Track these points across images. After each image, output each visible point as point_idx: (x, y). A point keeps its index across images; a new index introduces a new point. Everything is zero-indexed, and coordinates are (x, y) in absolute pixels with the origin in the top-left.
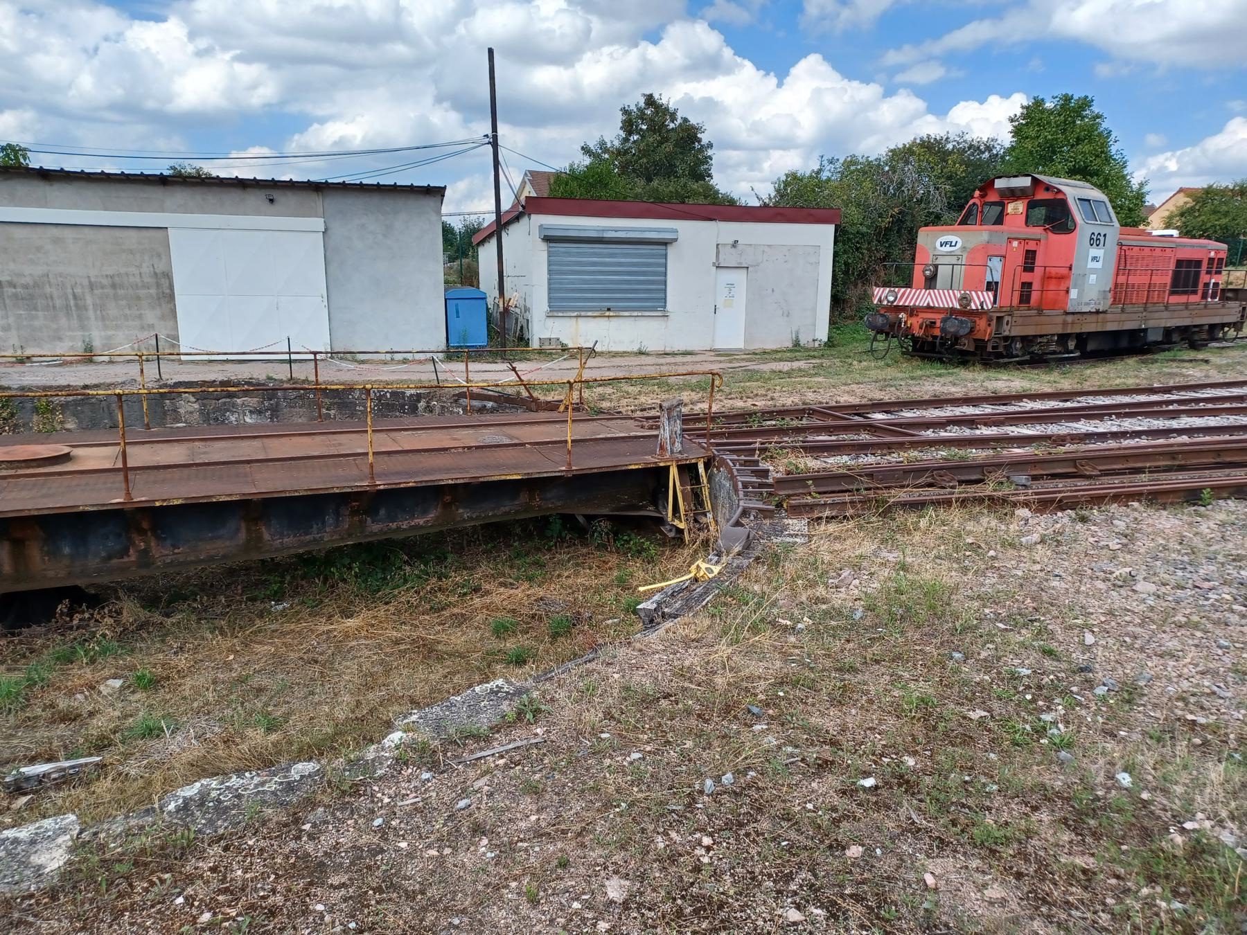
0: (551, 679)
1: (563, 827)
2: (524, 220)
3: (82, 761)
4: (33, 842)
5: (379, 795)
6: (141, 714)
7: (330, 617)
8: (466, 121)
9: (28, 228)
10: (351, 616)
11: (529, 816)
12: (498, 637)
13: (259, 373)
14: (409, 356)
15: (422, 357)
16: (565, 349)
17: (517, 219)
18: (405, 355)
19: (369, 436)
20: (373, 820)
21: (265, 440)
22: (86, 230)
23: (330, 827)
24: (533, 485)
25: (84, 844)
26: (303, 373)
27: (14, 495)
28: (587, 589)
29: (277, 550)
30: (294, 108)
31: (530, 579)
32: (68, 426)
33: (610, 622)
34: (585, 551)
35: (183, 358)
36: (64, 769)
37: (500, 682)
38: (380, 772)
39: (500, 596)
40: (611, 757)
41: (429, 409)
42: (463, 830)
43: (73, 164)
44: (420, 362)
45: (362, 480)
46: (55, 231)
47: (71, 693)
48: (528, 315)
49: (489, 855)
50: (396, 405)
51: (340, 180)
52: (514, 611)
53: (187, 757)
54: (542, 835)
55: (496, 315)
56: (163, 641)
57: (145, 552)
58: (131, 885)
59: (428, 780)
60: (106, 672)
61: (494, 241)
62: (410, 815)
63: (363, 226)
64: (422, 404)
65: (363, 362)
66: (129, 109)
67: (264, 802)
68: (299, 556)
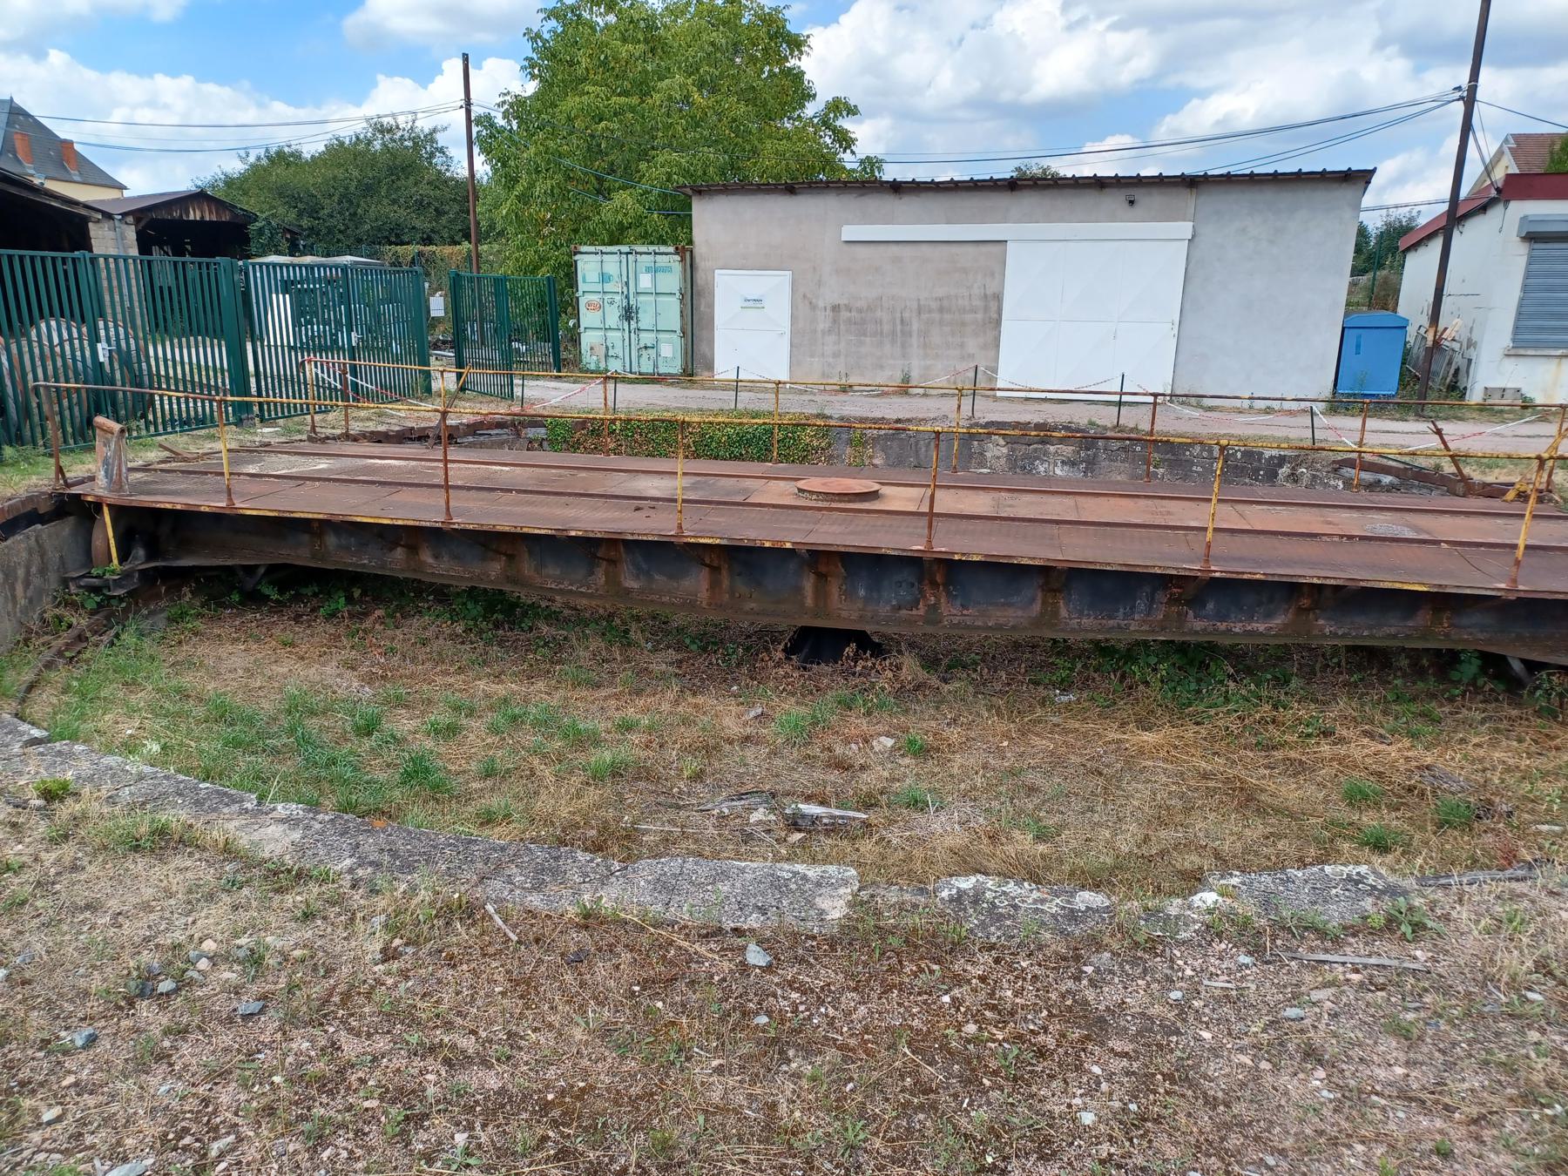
0: (1446, 887)
1: (1447, 1100)
2: (1496, 213)
3: (851, 814)
4: (819, 885)
5: (1180, 962)
6: (908, 781)
7: (1123, 724)
8: (1418, 70)
9: (871, 248)
10: (1149, 729)
11: (1389, 1065)
12: (1350, 804)
13: (1080, 416)
14: (1276, 405)
15: (1294, 406)
16: (1527, 405)
17: (1483, 209)
18: (1269, 403)
19: (1211, 507)
20: (1169, 990)
21: (1080, 499)
22: (924, 248)
23: (1116, 980)
24: (1444, 602)
25: (862, 903)
26: (1136, 419)
27: (825, 528)
28: (1508, 770)
29: (1073, 630)
30: (1171, 81)
31: (1414, 736)
32: (876, 461)
33: (1545, 828)
34: (1515, 713)
35: (999, 394)
36: (834, 817)
37: (1363, 869)
38: (1183, 935)
39: (1361, 749)
40: (1543, 1032)
41: (1294, 477)
42: (1291, 1047)
43: (922, 174)
44: (1290, 413)
45: (1192, 562)
46: (894, 248)
47: (847, 741)
48: (1472, 353)
49: (1325, 1093)
50: (1249, 468)
51: (1224, 171)
52: (1380, 775)
53: (949, 841)
54: (1411, 1099)
55: (1418, 352)
56: (937, 708)
57: (934, 608)
58: (900, 962)
59: (1247, 967)
60: (880, 728)
61: (1436, 246)
62: (1217, 1001)
63: (1244, 230)
64: (1284, 471)
65: (1210, 409)
66: (986, 105)
67: (1043, 923)
68: (1096, 643)
